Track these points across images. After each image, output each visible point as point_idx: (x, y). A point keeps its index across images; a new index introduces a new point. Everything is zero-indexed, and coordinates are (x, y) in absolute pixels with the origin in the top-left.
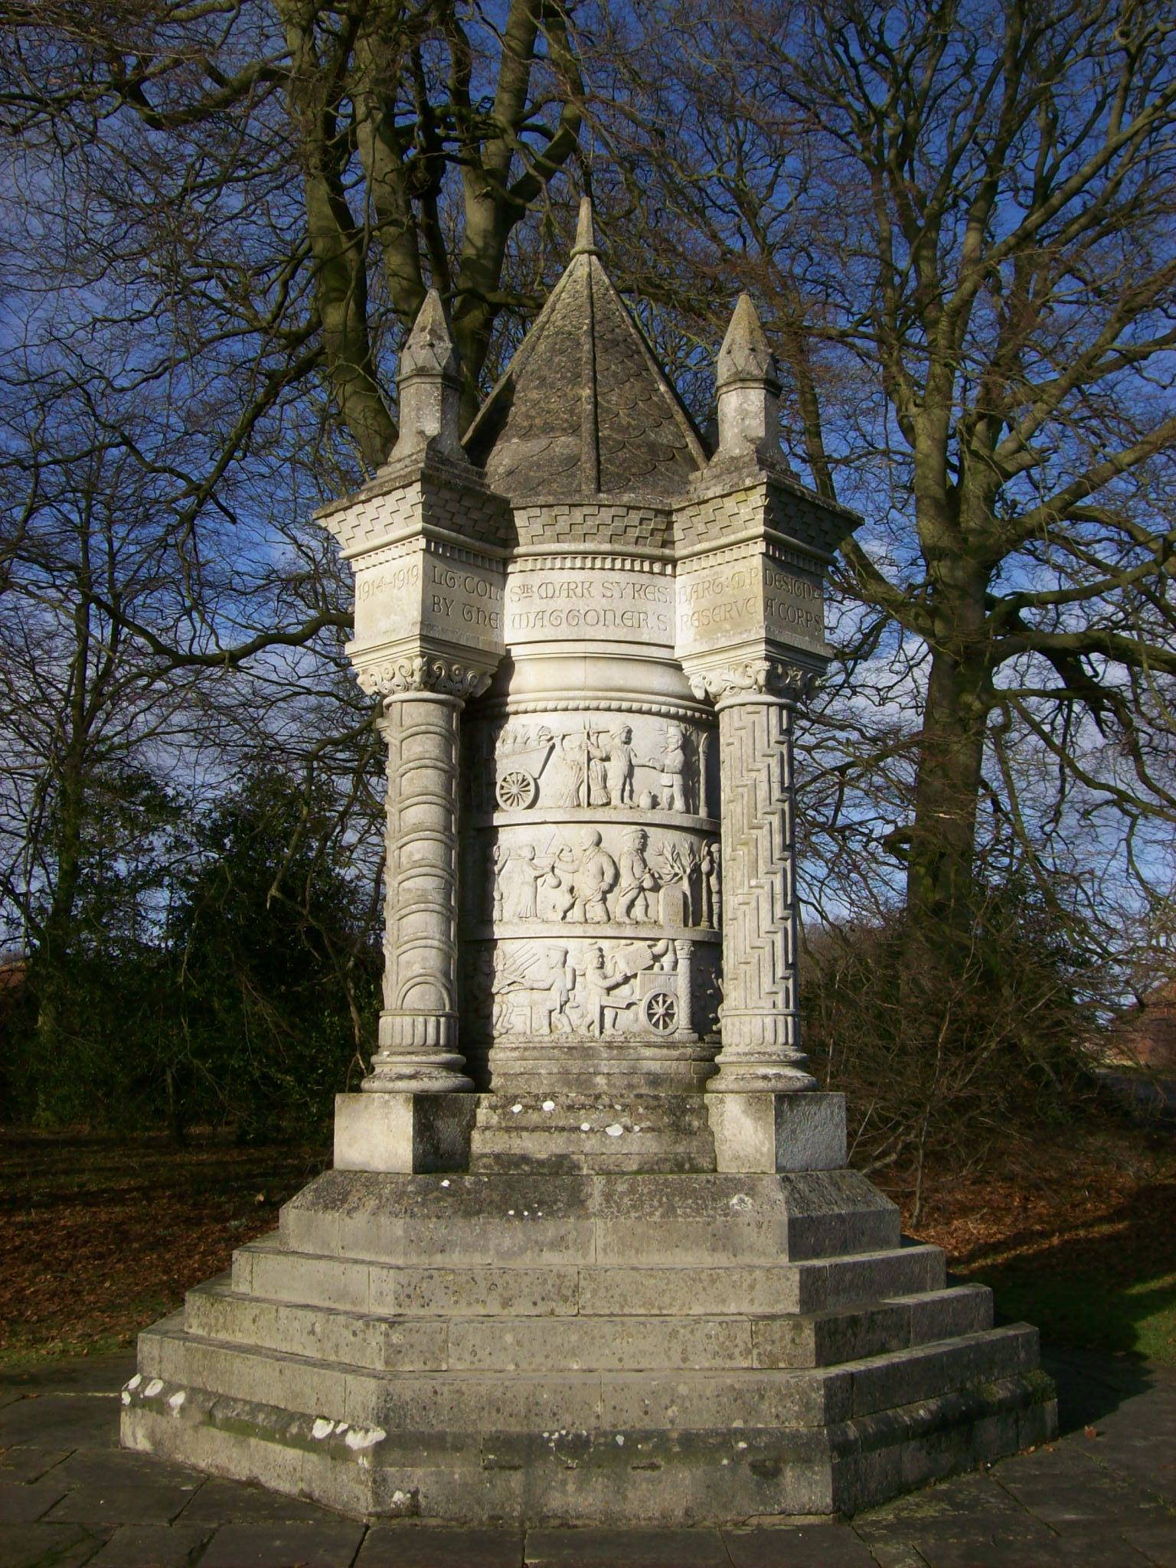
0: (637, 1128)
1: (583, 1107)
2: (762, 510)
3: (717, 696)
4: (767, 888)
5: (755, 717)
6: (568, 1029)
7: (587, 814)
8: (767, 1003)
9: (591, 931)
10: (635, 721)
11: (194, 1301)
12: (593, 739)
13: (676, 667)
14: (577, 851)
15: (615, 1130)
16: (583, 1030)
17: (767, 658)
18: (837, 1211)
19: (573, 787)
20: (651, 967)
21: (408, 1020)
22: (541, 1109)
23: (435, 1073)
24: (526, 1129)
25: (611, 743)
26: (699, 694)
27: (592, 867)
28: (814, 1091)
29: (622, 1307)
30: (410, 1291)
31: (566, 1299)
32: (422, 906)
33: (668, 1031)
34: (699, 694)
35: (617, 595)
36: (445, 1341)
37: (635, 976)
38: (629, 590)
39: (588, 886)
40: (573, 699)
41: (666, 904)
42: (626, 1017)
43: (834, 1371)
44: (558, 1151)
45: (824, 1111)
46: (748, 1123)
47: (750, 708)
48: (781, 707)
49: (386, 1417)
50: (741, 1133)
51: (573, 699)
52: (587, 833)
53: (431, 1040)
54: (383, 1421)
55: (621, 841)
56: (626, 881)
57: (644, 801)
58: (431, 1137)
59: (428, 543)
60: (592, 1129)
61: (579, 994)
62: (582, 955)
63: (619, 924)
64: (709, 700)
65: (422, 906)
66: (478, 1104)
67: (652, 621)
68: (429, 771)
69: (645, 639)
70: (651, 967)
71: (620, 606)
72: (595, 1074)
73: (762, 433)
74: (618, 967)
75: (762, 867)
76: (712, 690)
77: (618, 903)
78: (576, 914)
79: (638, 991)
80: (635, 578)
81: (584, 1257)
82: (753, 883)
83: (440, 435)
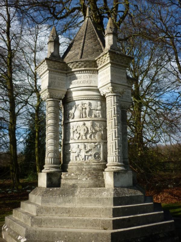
0: (88, 179)
1: (79, 174)
2: (109, 58)
3: (105, 95)
4: (114, 131)
5: (111, 98)
6: (79, 160)
7: (82, 119)
8: (114, 153)
9: (83, 141)
10: (91, 101)
11: (23, 204)
12: (83, 105)
13: (98, 90)
14: (81, 126)
15: (84, 179)
16: (81, 160)
17: (112, 86)
18: (127, 195)
19: (79, 114)
20: (95, 148)
21: (48, 159)
22: (71, 175)
23: (53, 169)
24: (68, 179)
25: (87, 106)
26: (102, 95)
27: (83, 129)
28: (125, 172)
29: (78, 215)
30: (39, 210)
31: (67, 213)
32: (51, 138)
33: (99, 160)
34: (102, 95)
35: (86, 77)
36: (42, 221)
37: (91, 149)
38: (88, 77)
39: (82, 133)
40: (86, 97)
41: (98, 136)
42: (90, 158)
43: (116, 231)
44: (74, 183)
45: (127, 175)
46: (109, 177)
47: (110, 96)
48: (114, 96)
49: (27, 236)
50: (109, 179)
51: (86, 97)
52: (82, 123)
53: (50, 162)
54: (26, 237)
55: (89, 124)
56: (90, 131)
57: (93, 116)
58: (51, 181)
59: (49, 71)
60: (80, 179)
61: (81, 154)
62: (82, 146)
63: (88, 140)
64: (104, 95)
65: (51, 138)
66: (62, 174)
67: (93, 82)
68: (52, 113)
69: (92, 85)
70: (95, 148)
71: (87, 80)
72: (83, 168)
73: (112, 43)
74: (88, 148)
75: (113, 127)
76: (104, 94)
77: (88, 136)
78: (80, 138)
79: (93, 153)
80: (89, 74)
81: (74, 204)
82: (111, 130)
83: (54, 52)
